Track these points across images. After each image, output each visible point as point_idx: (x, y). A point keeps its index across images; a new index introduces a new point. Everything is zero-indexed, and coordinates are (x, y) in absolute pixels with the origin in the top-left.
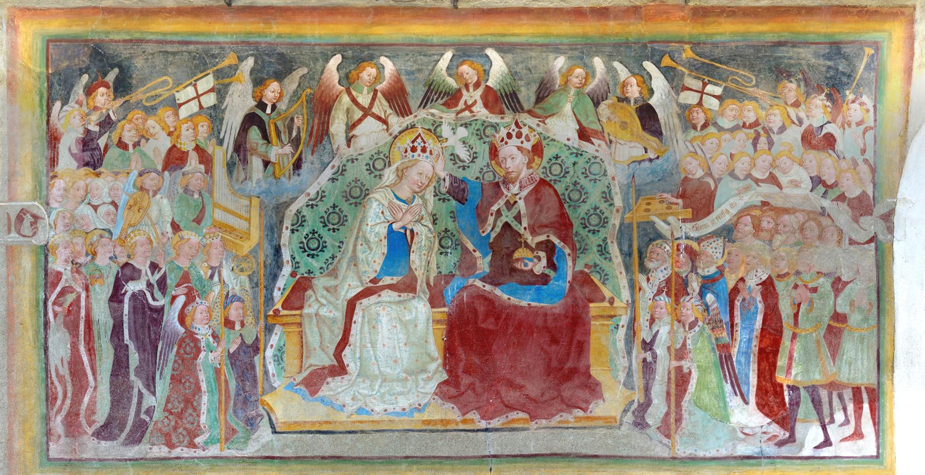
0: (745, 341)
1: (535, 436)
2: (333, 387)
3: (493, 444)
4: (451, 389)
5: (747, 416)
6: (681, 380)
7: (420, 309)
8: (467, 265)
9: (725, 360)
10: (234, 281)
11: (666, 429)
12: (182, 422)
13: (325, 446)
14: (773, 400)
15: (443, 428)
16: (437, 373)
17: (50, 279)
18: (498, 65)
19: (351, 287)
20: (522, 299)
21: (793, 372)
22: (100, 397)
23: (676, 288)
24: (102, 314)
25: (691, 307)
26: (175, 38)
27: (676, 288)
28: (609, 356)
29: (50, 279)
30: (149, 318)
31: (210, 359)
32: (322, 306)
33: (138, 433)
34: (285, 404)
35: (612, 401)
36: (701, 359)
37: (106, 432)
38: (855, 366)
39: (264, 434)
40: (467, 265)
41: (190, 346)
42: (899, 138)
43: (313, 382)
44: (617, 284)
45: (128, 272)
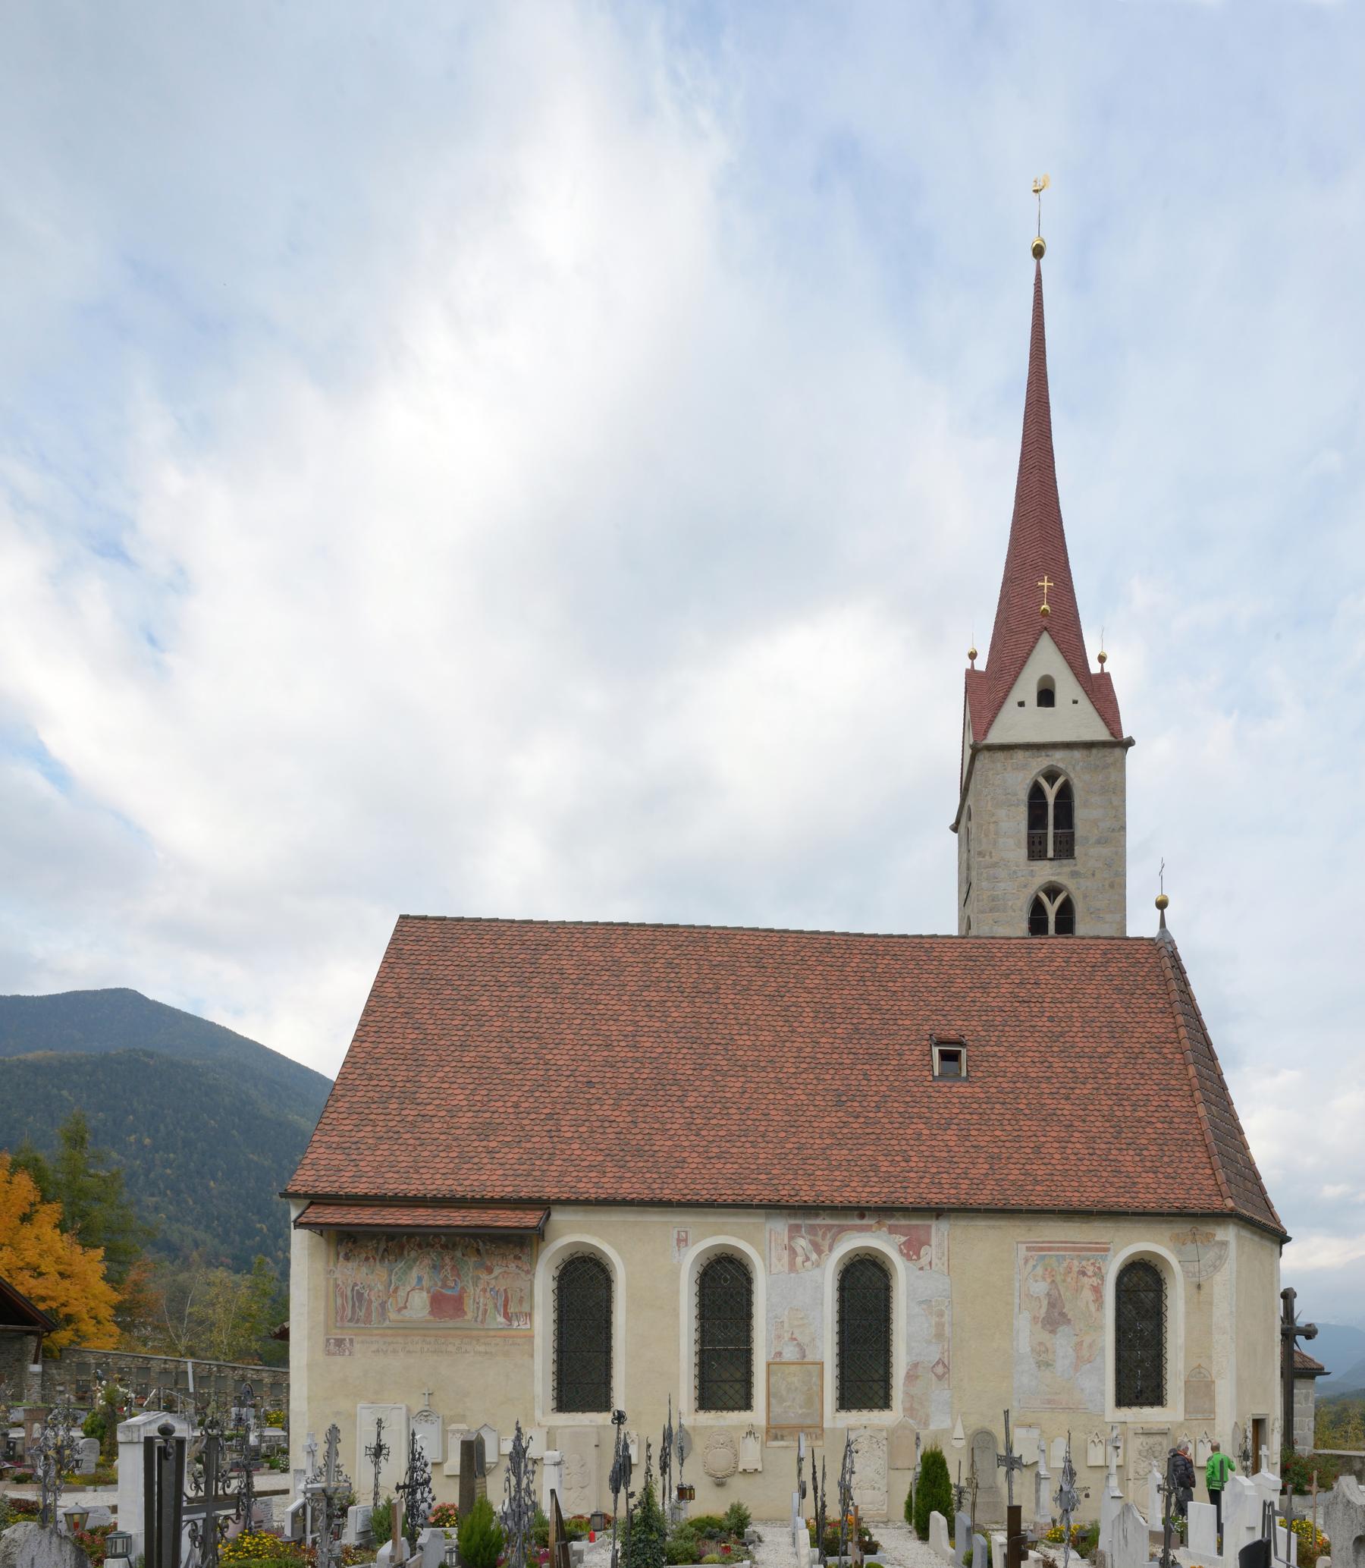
0: (501, 1302)
1: (451, 1324)
2: (404, 1311)
3: (441, 1325)
4: (432, 1313)
5: (501, 1319)
6: (486, 1311)
7: (425, 1294)
8: (436, 1284)
9: (496, 1307)
10: (380, 1287)
11: (483, 1322)
12: (368, 1319)
13: (402, 1325)
14: (506, 1315)
15: (427, 1321)
16: (428, 1309)
17: (337, 1286)
18: (444, 1239)
19: (408, 1288)
20: (449, 1292)
21: (511, 1310)
22: (349, 1312)
23: (484, 1290)
24: (349, 1293)
25: (488, 1294)
26: (965, 856)
27: (484, 1290)
28: (469, 1306)
29: (337, 1286)
30: (360, 1295)
31: (375, 1304)
32: (402, 1293)
33: (358, 1321)
34: (392, 1315)
35: (469, 1316)
36: (490, 1306)
37: (350, 1320)
38: (526, 1308)
39: (387, 1323)
40: (436, 1284)
41: (370, 1302)
42: (727, 1509)
43: (399, 1310)
44: (471, 1290)
45: (355, 1285)
